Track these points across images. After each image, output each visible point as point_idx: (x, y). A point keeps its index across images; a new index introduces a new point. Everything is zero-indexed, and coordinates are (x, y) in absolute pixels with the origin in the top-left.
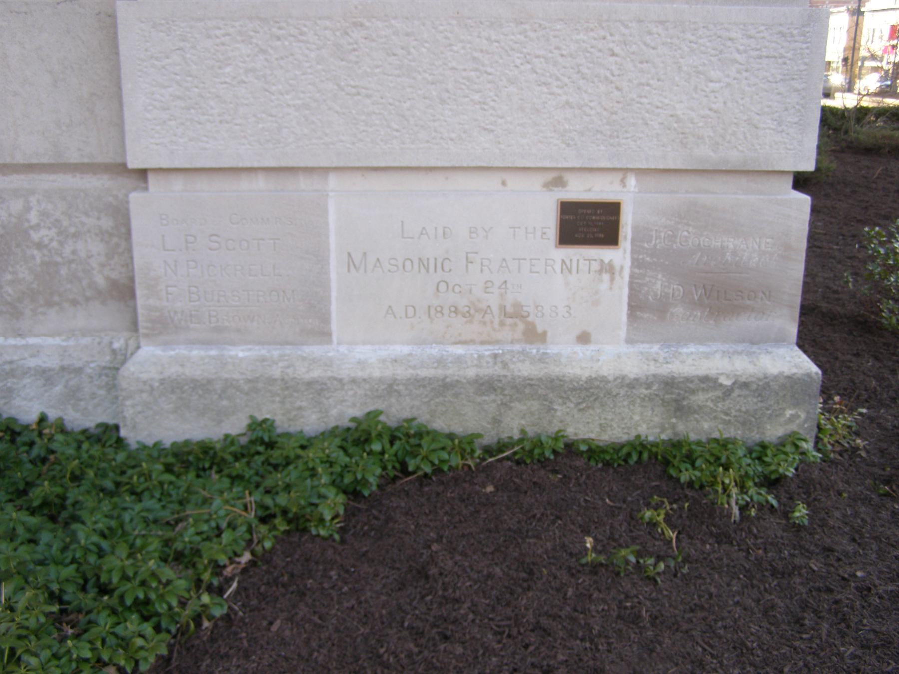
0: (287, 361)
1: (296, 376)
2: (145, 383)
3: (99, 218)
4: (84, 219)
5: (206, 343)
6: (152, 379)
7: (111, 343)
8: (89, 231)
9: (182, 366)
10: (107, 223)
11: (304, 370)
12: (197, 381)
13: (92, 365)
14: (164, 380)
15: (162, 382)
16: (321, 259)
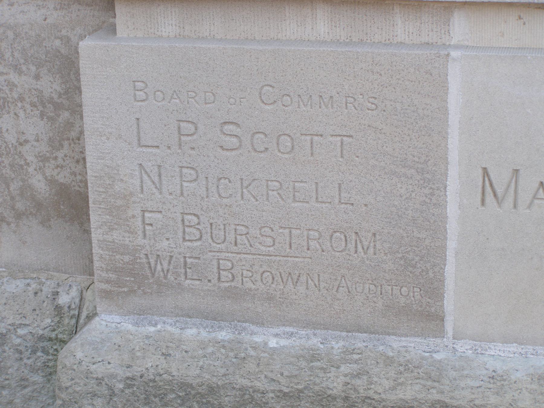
0: (356, 362)
1: (371, 393)
2: (99, 381)
3: (37, 77)
4: (13, 77)
5: (214, 318)
6: (113, 376)
7: (56, 294)
8: (21, 99)
9: (166, 355)
10: (50, 85)
11: (387, 384)
12: (191, 386)
13: (20, 332)
14: (132, 379)
15: (129, 382)
16: (429, 176)
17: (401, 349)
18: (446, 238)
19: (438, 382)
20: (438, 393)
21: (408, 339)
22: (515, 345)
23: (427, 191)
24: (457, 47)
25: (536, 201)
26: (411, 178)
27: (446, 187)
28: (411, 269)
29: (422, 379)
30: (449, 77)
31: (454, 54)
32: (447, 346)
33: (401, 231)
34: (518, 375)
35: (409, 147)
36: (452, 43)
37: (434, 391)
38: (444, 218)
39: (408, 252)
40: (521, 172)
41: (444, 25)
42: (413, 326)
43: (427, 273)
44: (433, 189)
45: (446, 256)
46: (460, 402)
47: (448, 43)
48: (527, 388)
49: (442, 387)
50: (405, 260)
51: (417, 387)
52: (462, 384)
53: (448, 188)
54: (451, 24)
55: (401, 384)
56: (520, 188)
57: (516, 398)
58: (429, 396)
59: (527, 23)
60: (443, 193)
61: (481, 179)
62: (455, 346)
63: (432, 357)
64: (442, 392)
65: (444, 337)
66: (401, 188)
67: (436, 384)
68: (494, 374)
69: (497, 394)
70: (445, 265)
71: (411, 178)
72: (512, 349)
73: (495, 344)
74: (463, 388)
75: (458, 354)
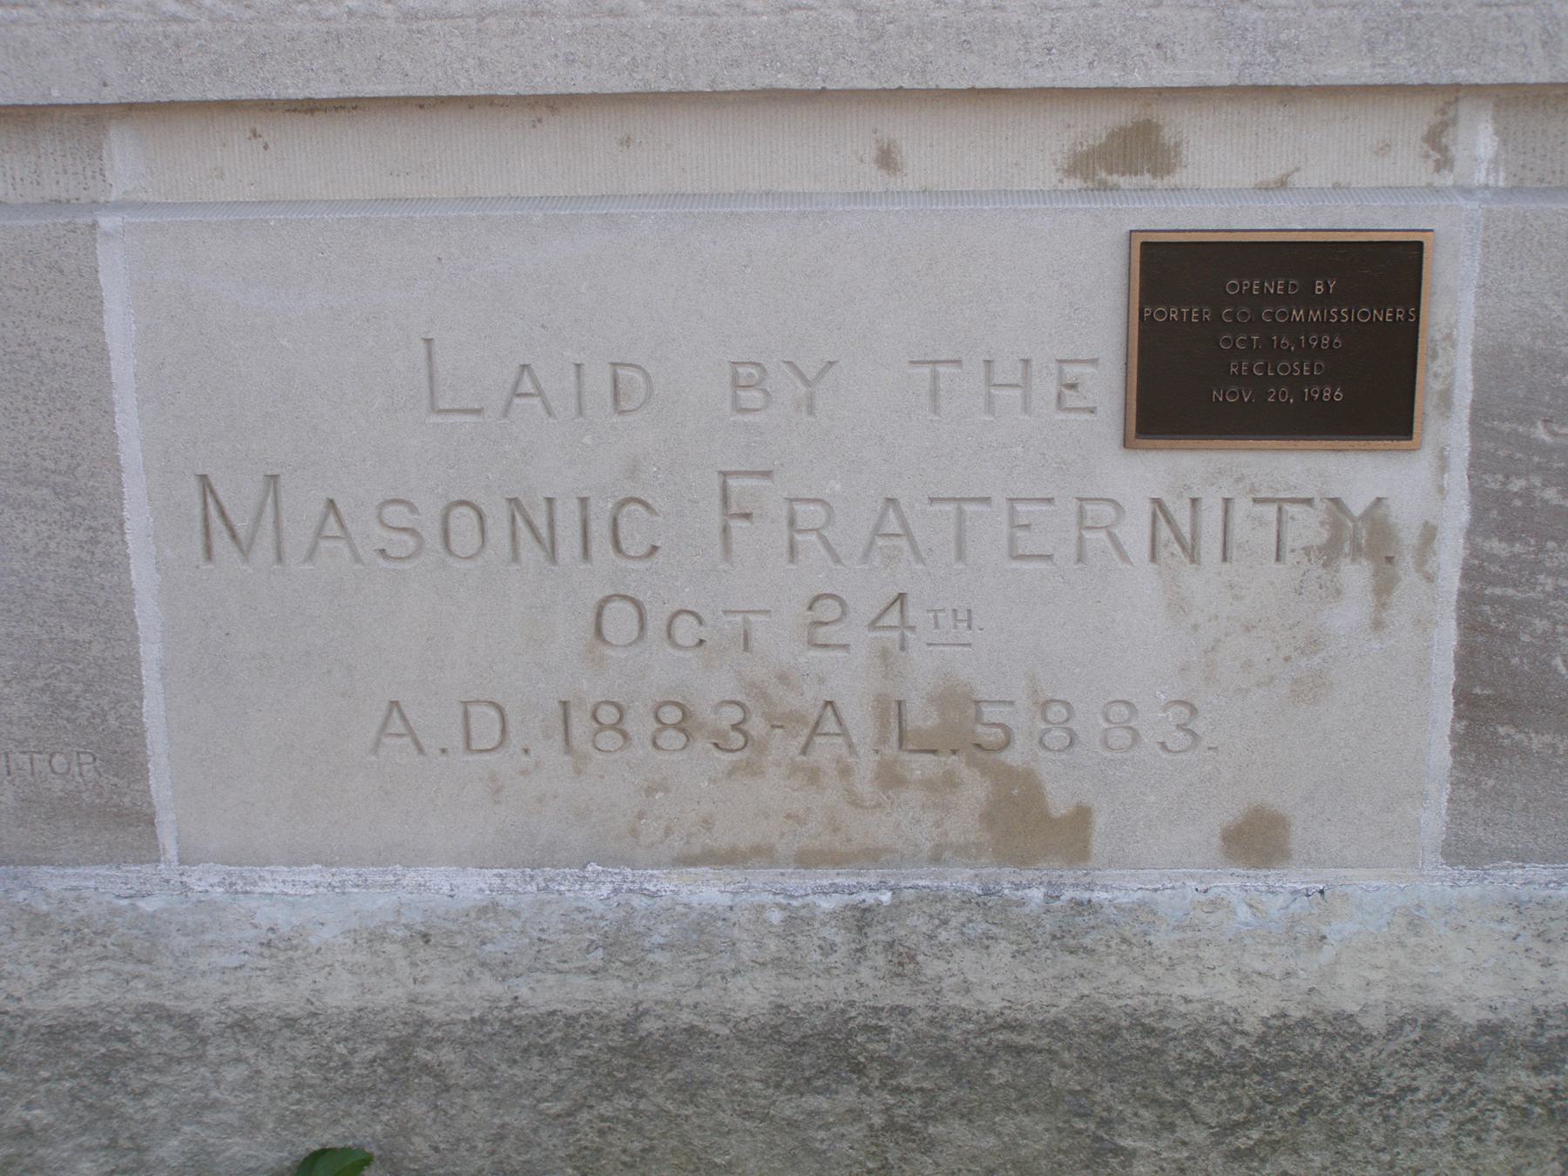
11: (35, 976)
17: (68, 894)
18: (136, 639)
19: (148, 962)
20: (148, 987)
21: (80, 870)
22: (316, 867)
23: (81, 535)
24: (119, 207)
25: (324, 544)
26: (44, 507)
27: (121, 524)
28: (66, 713)
29: (113, 958)
30: (100, 276)
31: (107, 222)
32: (167, 881)
33: (36, 629)
34: (326, 934)
35: (31, 438)
36: (112, 199)
37: (140, 985)
38: (125, 593)
39: (56, 676)
40: (283, 480)
41: (90, 157)
42: (88, 840)
43: (104, 720)
44: (95, 530)
45: (140, 678)
46: (198, 1005)
47: (102, 199)
48: (344, 963)
49: (157, 973)
50: (53, 692)
51: (102, 979)
52: (202, 964)
53: (127, 525)
54: (105, 155)
55: (67, 974)
56: (284, 515)
57: (319, 986)
58: (129, 996)
59: (271, 146)
60: (117, 538)
61: (197, 500)
62: (184, 879)
63: (134, 907)
64: (158, 986)
65: (159, 861)
66: (24, 531)
67: (144, 968)
68: (271, 936)
69: (279, 979)
70: (141, 699)
71: (44, 507)
72: (310, 878)
73: (272, 868)
74: (203, 974)
75: (193, 897)
